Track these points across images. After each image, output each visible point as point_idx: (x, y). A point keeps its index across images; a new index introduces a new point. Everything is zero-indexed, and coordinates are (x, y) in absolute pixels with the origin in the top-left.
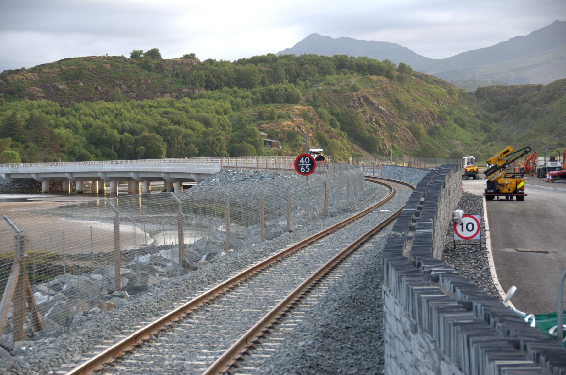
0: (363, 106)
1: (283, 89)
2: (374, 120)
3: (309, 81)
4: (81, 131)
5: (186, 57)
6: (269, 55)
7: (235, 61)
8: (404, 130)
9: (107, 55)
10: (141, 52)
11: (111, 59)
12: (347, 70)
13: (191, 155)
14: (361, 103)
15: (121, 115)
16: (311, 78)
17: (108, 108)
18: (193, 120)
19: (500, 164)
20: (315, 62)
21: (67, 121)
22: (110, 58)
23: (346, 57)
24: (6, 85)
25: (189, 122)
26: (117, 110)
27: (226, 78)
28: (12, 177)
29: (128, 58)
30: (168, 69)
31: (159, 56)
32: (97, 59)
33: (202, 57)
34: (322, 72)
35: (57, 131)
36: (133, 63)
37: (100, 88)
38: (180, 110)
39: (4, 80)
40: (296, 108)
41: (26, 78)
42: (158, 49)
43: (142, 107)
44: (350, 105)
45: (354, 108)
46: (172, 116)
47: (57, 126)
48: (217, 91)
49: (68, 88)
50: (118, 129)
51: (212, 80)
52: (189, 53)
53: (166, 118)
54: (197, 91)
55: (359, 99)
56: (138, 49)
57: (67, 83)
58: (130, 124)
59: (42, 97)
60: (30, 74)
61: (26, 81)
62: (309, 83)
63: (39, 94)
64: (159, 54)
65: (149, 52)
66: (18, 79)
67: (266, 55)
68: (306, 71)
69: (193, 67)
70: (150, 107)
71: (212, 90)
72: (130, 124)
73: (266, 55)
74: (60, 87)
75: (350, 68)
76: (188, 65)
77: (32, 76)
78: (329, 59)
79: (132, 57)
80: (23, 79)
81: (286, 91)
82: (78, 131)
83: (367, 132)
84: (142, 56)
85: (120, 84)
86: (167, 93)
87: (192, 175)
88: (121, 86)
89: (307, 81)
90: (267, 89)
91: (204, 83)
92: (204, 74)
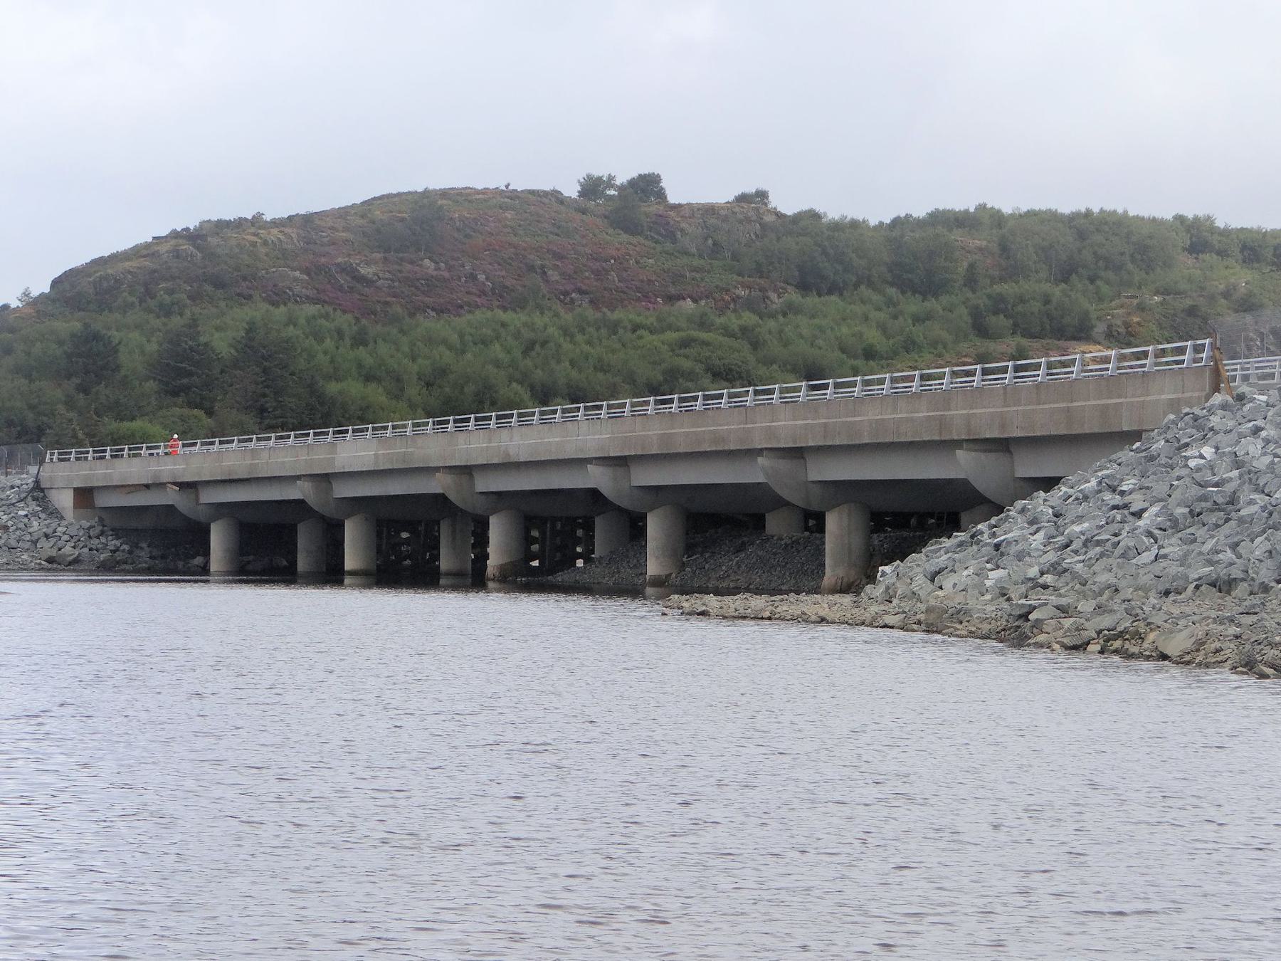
3: (1108, 282)
4: (413, 391)
5: (743, 198)
6: (982, 208)
9: (507, 186)
10: (610, 182)
11: (518, 197)
12: (1215, 257)
15: (544, 344)
16: (1110, 275)
17: (504, 325)
18: (775, 367)
19: (850, 621)
21: (369, 361)
22: (514, 195)
24: (203, 258)
26: (533, 330)
28: (104, 501)
30: (689, 229)
31: (661, 195)
32: (477, 197)
33: (786, 202)
35: (333, 388)
36: (584, 212)
37: (482, 277)
38: (732, 335)
39: (198, 248)
41: (265, 243)
42: (658, 176)
43: (614, 327)
46: (708, 354)
47: (336, 376)
48: (833, 298)
49: (387, 275)
50: (532, 388)
52: (751, 190)
53: (687, 357)
54: (774, 296)
56: (600, 171)
57: (385, 258)
58: (574, 374)
59: (307, 297)
60: (275, 231)
61: (263, 250)
62: (1105, 289)
63: (297, 289)
64: (662, 189)
65: (632, 183)
66: (238, 245)
68: (1095, 253)
69: (764, 226)
70: (636, 328)
71: (820, 295)
72: (574, 374)
73: (972, 210)
74: (363, 272)
76: (748, 220)
77: (282, 237)
79: (583, 193)
80: (254, 244)
81: (1047, 302)
82: (402, 390)
84: (612, 192)
85: (543, 267)
86: (684, 299)
87: (960, 453)
88: (545, 273)
89: (1099, 283)
91: (797, 273)
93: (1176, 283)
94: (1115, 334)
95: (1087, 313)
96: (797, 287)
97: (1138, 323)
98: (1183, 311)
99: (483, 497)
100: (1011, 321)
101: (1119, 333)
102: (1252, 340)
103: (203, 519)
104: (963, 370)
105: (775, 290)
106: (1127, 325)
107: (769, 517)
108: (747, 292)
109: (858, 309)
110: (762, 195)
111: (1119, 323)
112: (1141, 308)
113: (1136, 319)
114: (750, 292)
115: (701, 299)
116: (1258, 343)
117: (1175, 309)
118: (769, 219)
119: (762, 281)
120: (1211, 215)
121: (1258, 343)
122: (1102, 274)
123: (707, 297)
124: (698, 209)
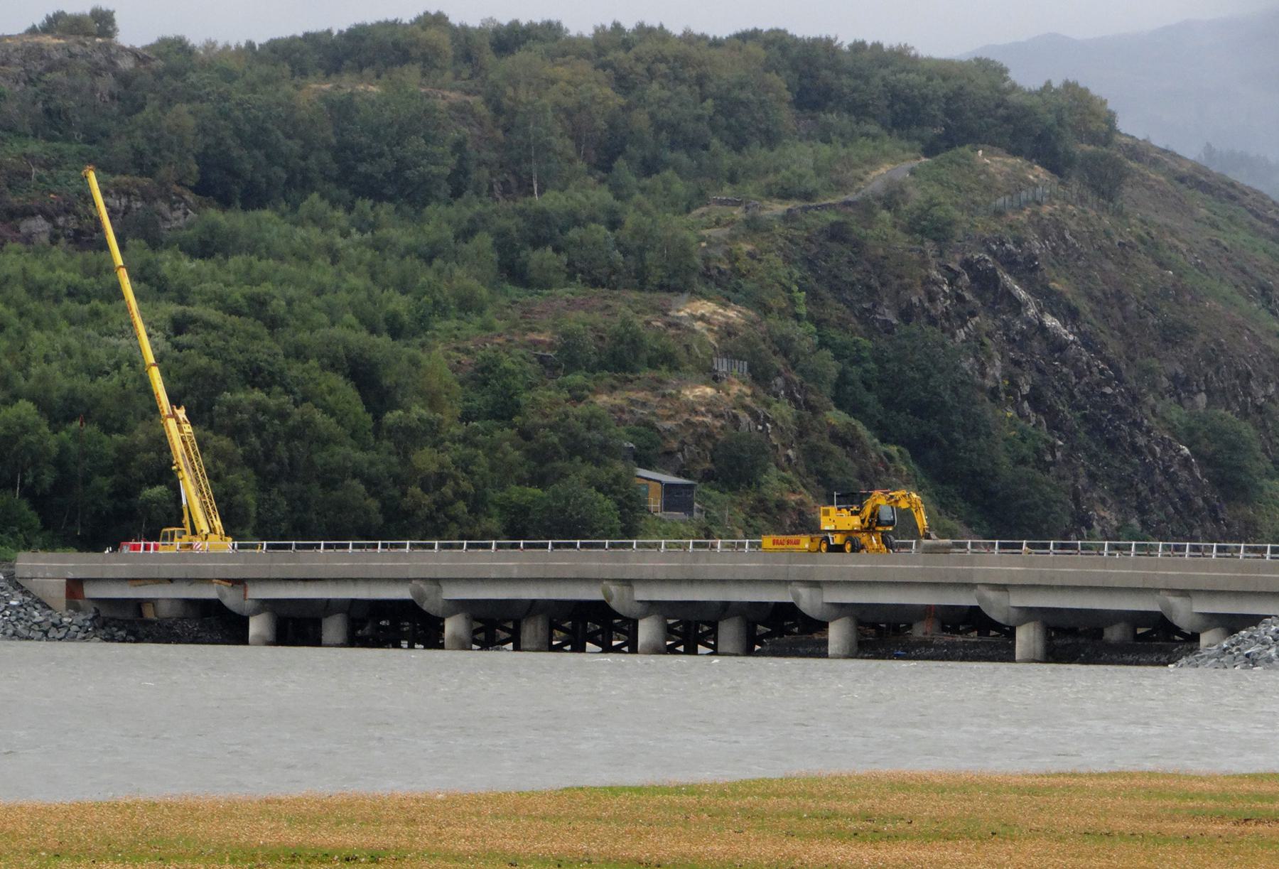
0: (973, 314)
1: (602, 216)
2: (1026, 389)
7: (250, 45)
8: (1167, 446)
13: (366, 533)
14: (960, 298)
16: (682, 157)
20: (691, 73)
23: (785, 32)
25: (294, 373)
27: (295, 146)
28: (91, 592)
29: (131, 69)
34: (729, 127)
38: (236, 312)
40: (694, 318)
44: (911, 305)
45: (933, 321)
51: (235, 154)
55: (953, 277)
67: (458, 25)
75: (860, 110)
78: (716, 43)
83: (1004, 459)
86: (33, 215)
90: (521, 213)
91: (195, 168)
92: (191, 122)
93: (801, 176)
94: (714, 272)
95: (685, 240)
96: (196, 190)
97: (751, 255)
98: (822, 231)
99: (640, 605)
100: (564, 258)
101: (720, 272)
102: (935, 283)
103: (245, 614)
104: (111, 218)
105: (166, 198)
106: (733, 258)
107: (830, 625)
108: (124, 201)
109: (314, 234)
110: (103, 21)
111: (719, 253)
112: (754, 226)
113: (747, 247)
114: (129, 201)
115: (58, 215)
116: (945, 288)
117: (807, 229)
118: (126, 64)
119: (145, 182)
120: (832, 37)
121: (945, 288)
122: (669, 155)
123: (67, 212)
124: (16, 50)
